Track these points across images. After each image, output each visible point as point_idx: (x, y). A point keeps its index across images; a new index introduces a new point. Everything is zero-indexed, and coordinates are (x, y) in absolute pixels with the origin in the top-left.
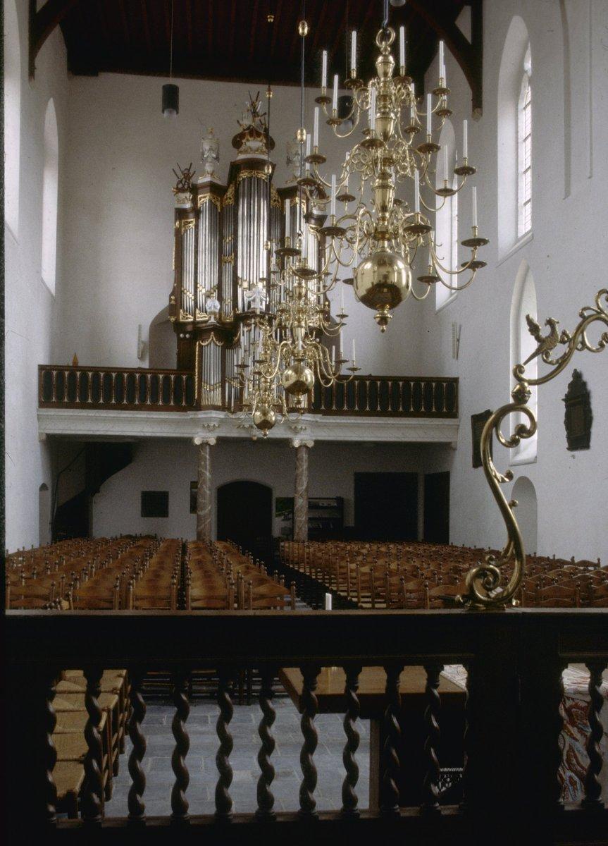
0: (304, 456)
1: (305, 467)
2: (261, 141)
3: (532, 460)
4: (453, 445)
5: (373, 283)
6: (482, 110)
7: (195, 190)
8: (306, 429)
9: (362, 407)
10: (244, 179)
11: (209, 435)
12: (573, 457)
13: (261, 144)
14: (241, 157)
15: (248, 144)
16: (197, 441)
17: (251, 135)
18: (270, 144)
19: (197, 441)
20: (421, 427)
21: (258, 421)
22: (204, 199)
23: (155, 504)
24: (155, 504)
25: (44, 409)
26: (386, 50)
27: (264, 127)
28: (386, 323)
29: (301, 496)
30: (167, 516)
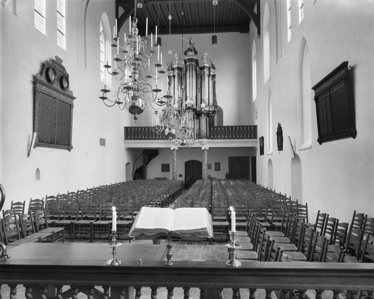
0: (206, 152)
1: (206, 156)
2: (193, 52)
3: (310, 147)
4: (256, 148)
5: (130, 106)
6: (260, 36)
7: (173, 69)
8: (206, 144)
9: (228, 136)
10: (188, 65)
11: (176, 147)
12: (279, 153)
13: (192, 53)
14: (187, 58)
15: (189, 53)
16: (172, 149)
17: (189, 51)
18: (196, 53)
19: (172, 149)
20: (245, 142)
21: (181, 143)
22: (176, 72)
23: (165, 168)
24: (165, 168)
25: (126, 140)
26: (135, 26)
27: (193, 48)
28: (137, 119)
29: (205, 165)
30: (169, 172)
